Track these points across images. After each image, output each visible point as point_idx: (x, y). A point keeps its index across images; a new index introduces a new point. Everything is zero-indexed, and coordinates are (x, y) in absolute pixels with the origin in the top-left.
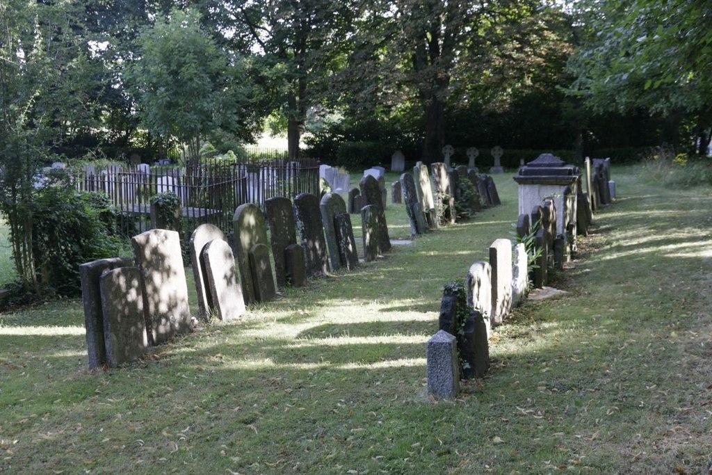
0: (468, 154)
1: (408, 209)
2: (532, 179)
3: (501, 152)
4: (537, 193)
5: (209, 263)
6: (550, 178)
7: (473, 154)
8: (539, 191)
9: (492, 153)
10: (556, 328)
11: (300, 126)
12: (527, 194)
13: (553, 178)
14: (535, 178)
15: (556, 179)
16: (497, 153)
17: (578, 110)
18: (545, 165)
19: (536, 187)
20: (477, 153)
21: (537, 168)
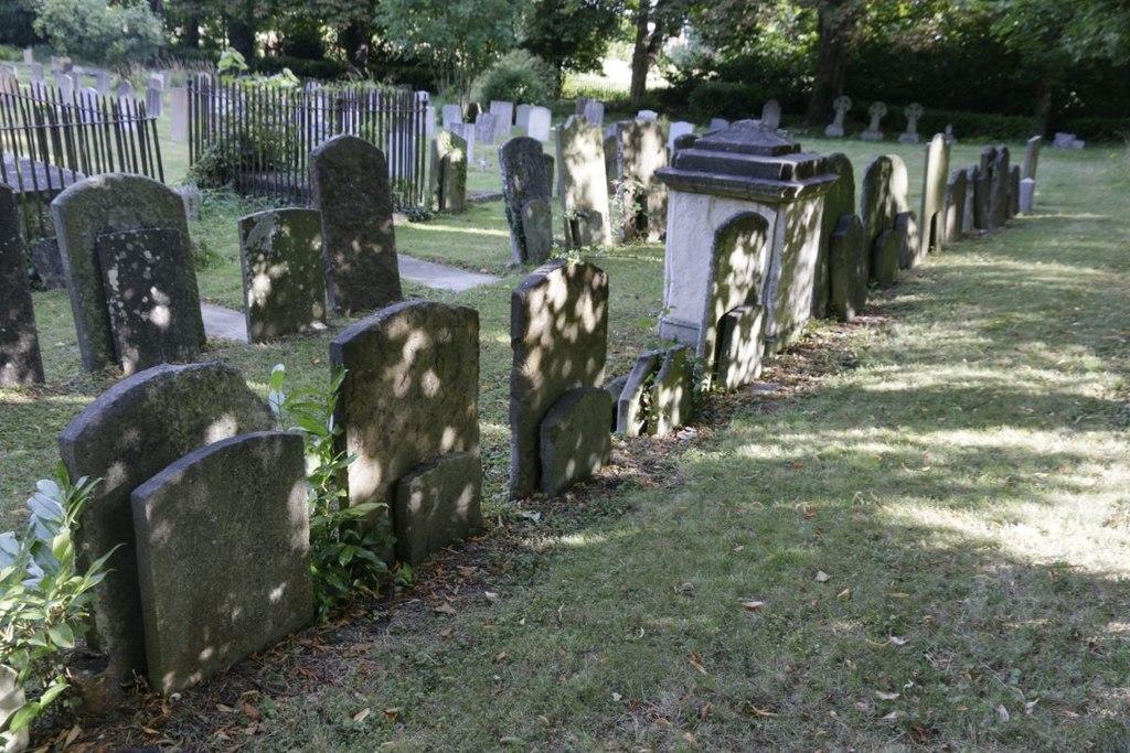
0: (906, 114)
1: (508, 212)
2: (694, 180)
3: (920, 113)
4: (704, 216)
5: (939, 173)
6: (729, 183)
7: (878, 111)
8: (709, 211)
9: (907, 112)
10: (869, 384)
11: (651, 54)
12: (682, 215)
13: (739, 184)
14: (704, 180)
15: (747, 186)
16: (914, 112)
17: (1049, 54)
18: (721, 147)
19: (704, 200)
20: (884, 112)
21: (709, 154)
